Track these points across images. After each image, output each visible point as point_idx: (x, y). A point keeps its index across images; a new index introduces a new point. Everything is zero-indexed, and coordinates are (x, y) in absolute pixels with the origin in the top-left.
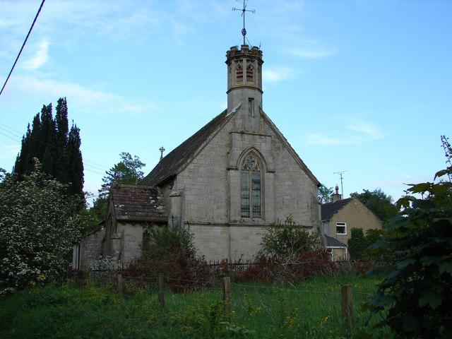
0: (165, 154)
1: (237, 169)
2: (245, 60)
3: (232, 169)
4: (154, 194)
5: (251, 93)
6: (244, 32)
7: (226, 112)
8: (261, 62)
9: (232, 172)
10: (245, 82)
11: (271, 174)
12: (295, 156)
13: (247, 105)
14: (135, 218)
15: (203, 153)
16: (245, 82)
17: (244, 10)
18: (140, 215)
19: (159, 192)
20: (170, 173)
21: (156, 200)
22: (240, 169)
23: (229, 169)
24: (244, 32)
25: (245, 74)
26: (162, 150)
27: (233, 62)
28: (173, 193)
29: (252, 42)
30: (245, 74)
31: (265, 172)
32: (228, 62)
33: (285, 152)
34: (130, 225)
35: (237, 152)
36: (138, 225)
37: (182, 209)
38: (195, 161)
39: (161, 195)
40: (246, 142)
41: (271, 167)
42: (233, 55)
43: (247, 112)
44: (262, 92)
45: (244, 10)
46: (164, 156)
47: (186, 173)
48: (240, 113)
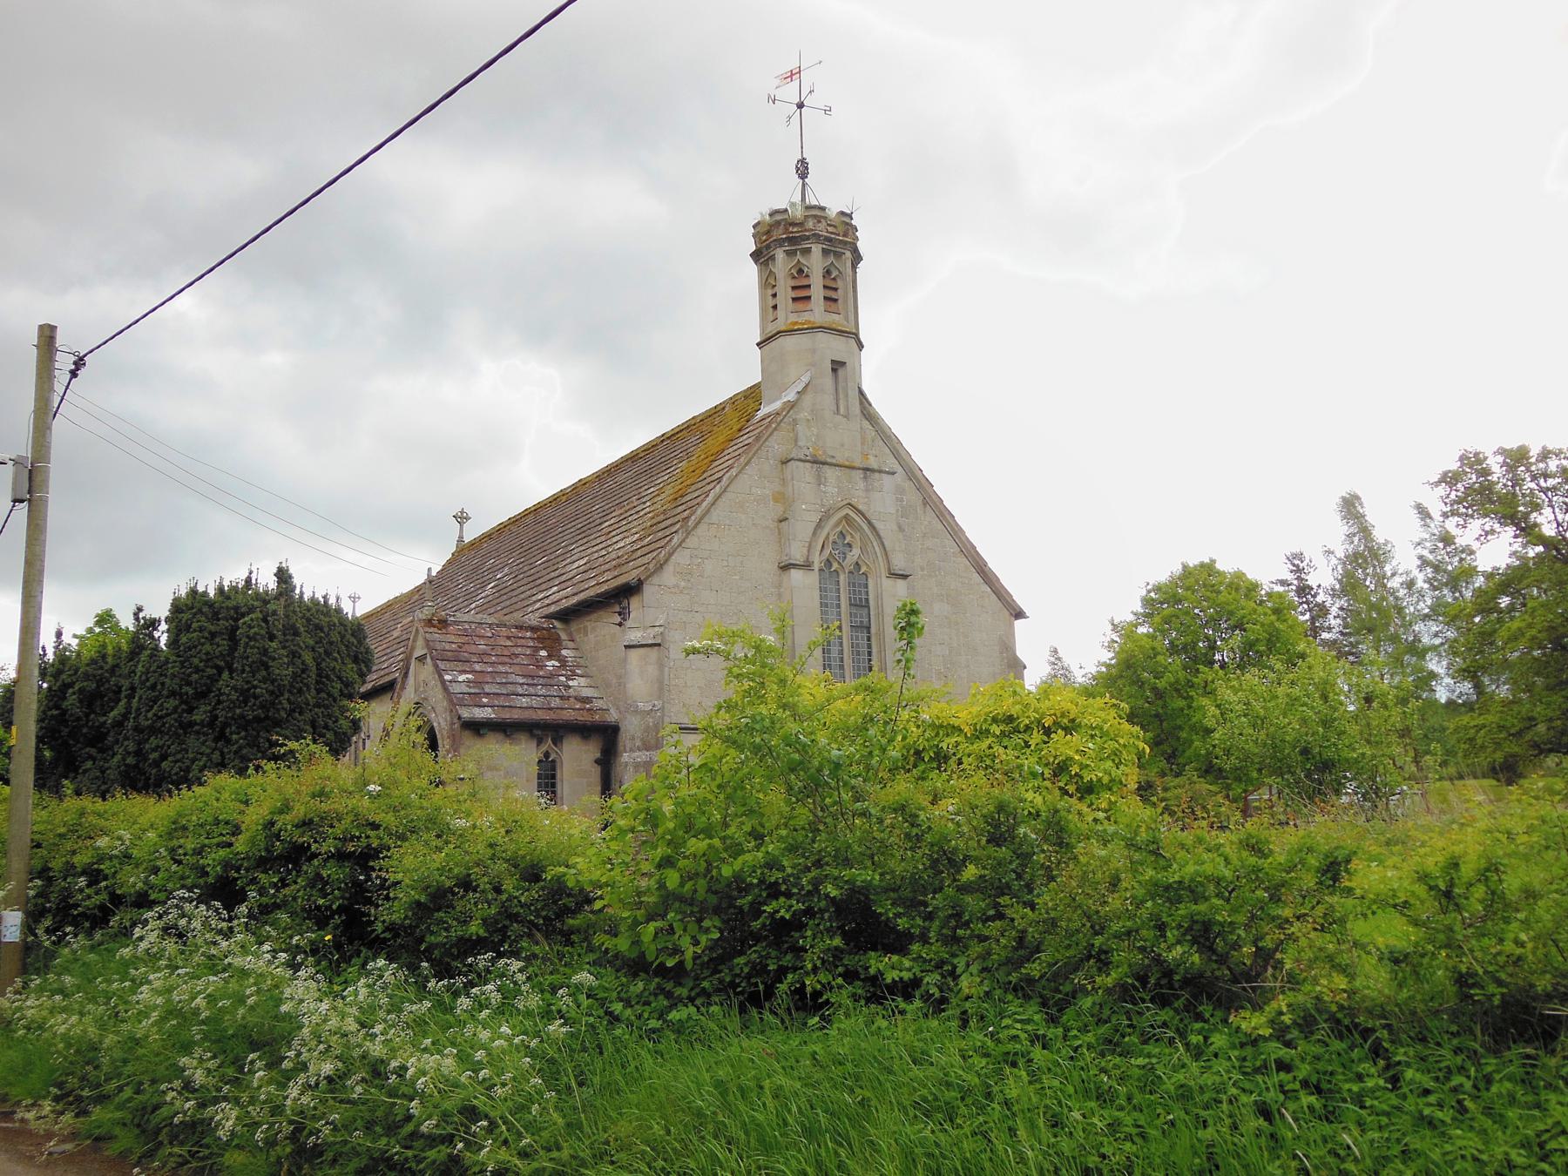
0: (472, 532)
1: (807, 566)
2: (816, 249)
3: (794, 566)
4: (551, 642)
5: (834, 347)
6: (803, 170)
7: (753, 395)
8: (857, 258)
9: (795, 574)
10: (817, 311)
11: (900, 582)
12: (955, 532)
13: (828, 380)
14: (507, 715)
15: (715, 516)
16: (817, 311)
17: (800, 106)
18: (527, 704)
19: (563, 636)
20: (629, 577)
21: (563, 662)
22: (816, 567)
23: (786, 568)
24: (803, 170)
25: (817, 292)
26: (461, 518)
27: (780, 254)
28: (635, 636)
29: (830, 197)
30: (817, 292)
31: (884, 573)
32: (760, 256)
33: (929, 518)
34: (500, 736)
35: (803, 526)
36: (523, 737)
37: (661, 688)
38: (692, 541)
39: (570, 644)
40: (831, 489)
41: (899, 563)
42: (779, 234)
43: (828, 400)
44: (861, 346)
45: (800, 106)
46: (467, 540)
47: (668, 576)
48: (808, 400)
